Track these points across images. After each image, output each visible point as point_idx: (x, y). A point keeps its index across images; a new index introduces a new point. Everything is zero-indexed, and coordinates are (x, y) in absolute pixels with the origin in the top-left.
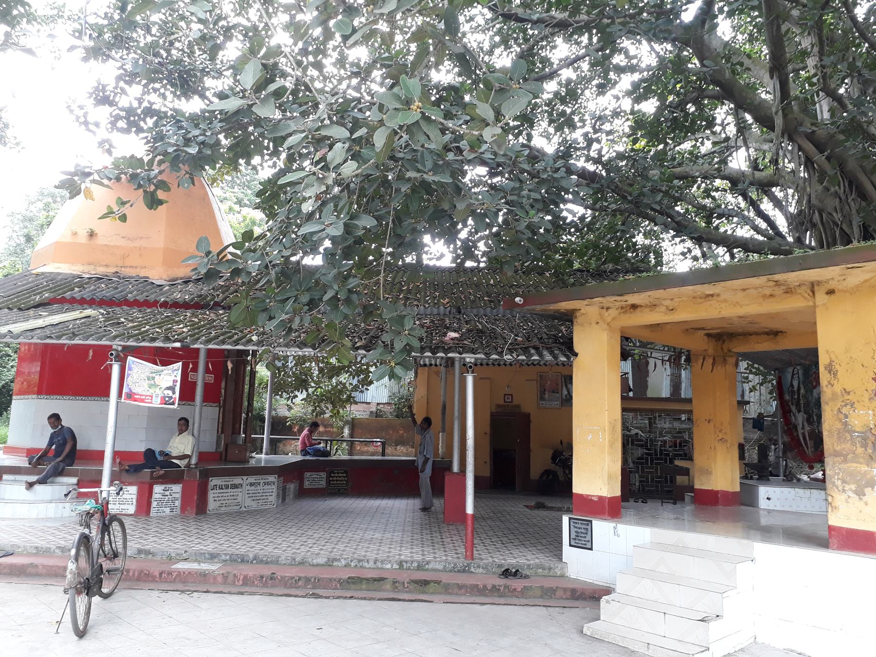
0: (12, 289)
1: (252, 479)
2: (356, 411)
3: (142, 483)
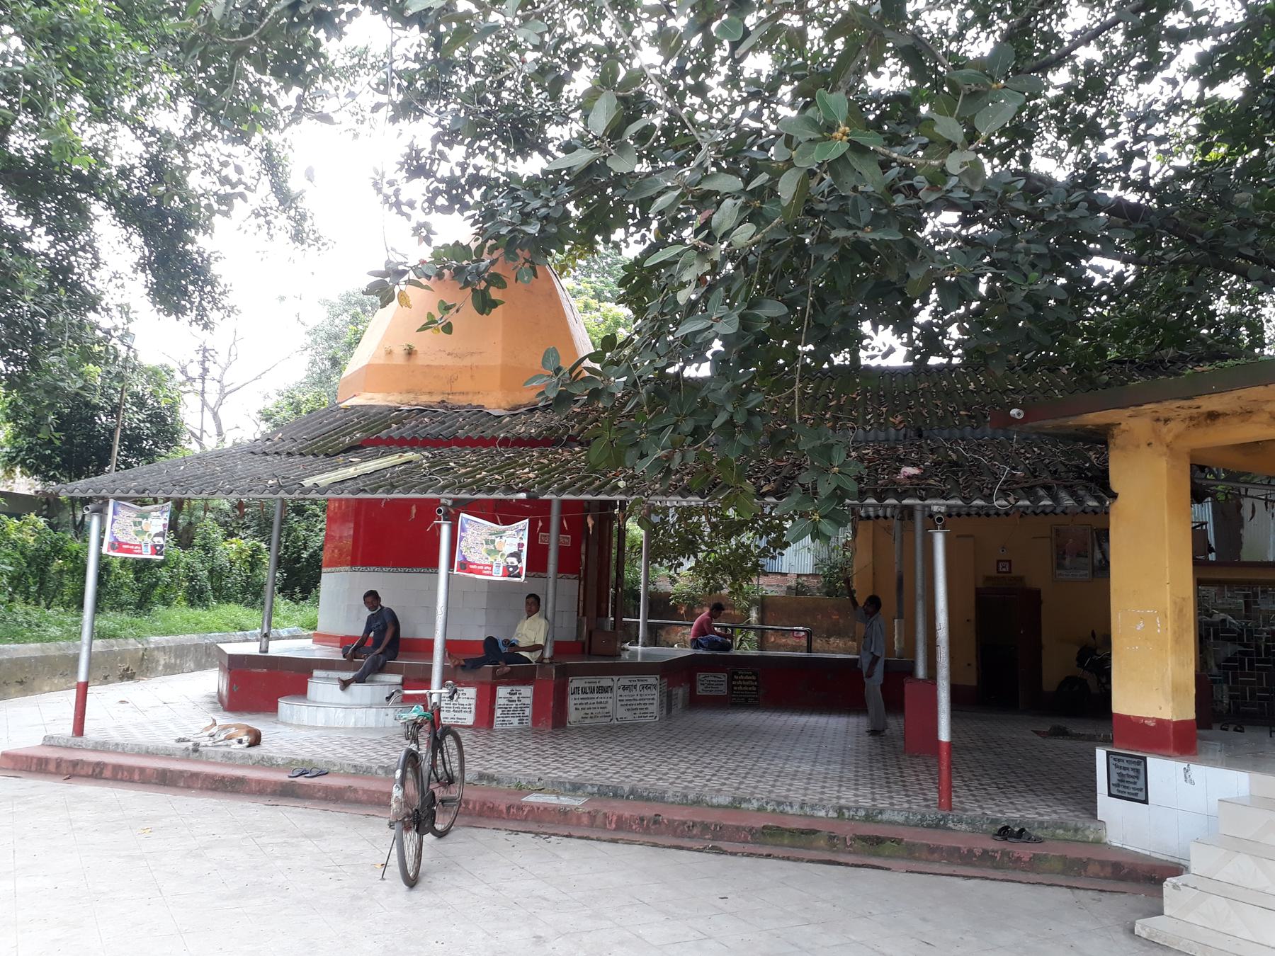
0: (316, 429)
1: (625, 681)
2: (767, 586)
3: (482, 683)
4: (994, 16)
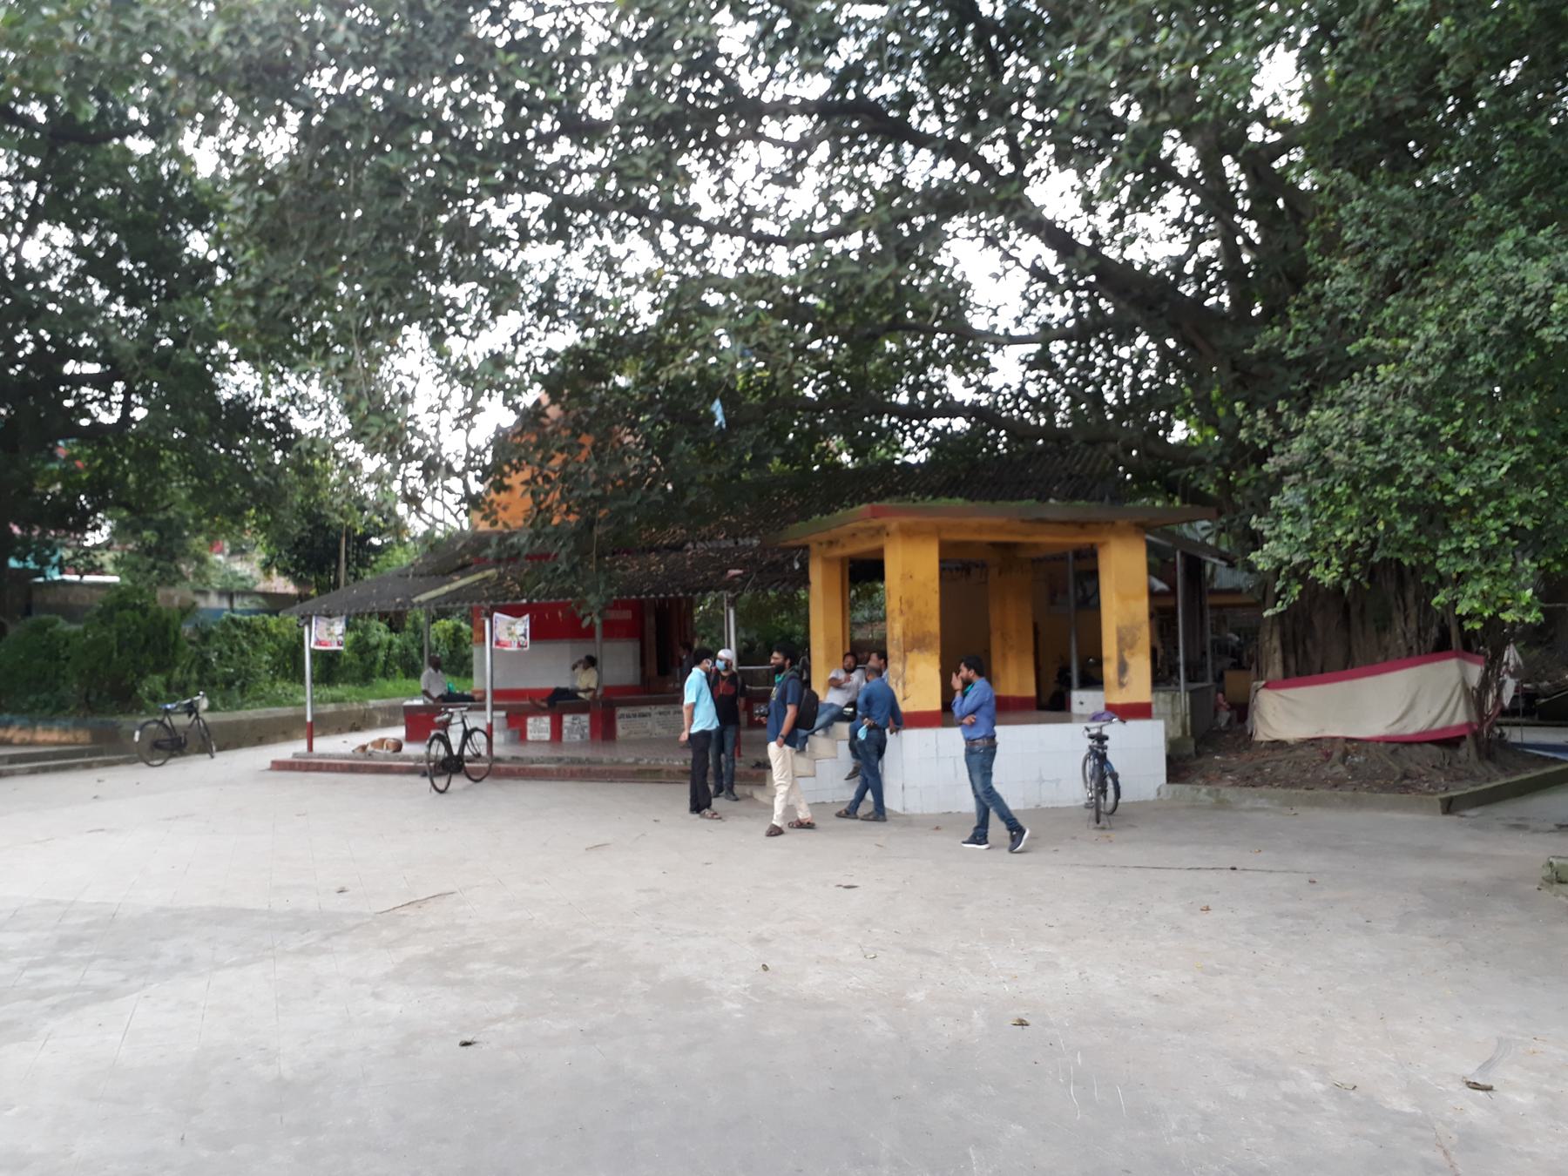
1: (661, 708)
4: (507, 481)
